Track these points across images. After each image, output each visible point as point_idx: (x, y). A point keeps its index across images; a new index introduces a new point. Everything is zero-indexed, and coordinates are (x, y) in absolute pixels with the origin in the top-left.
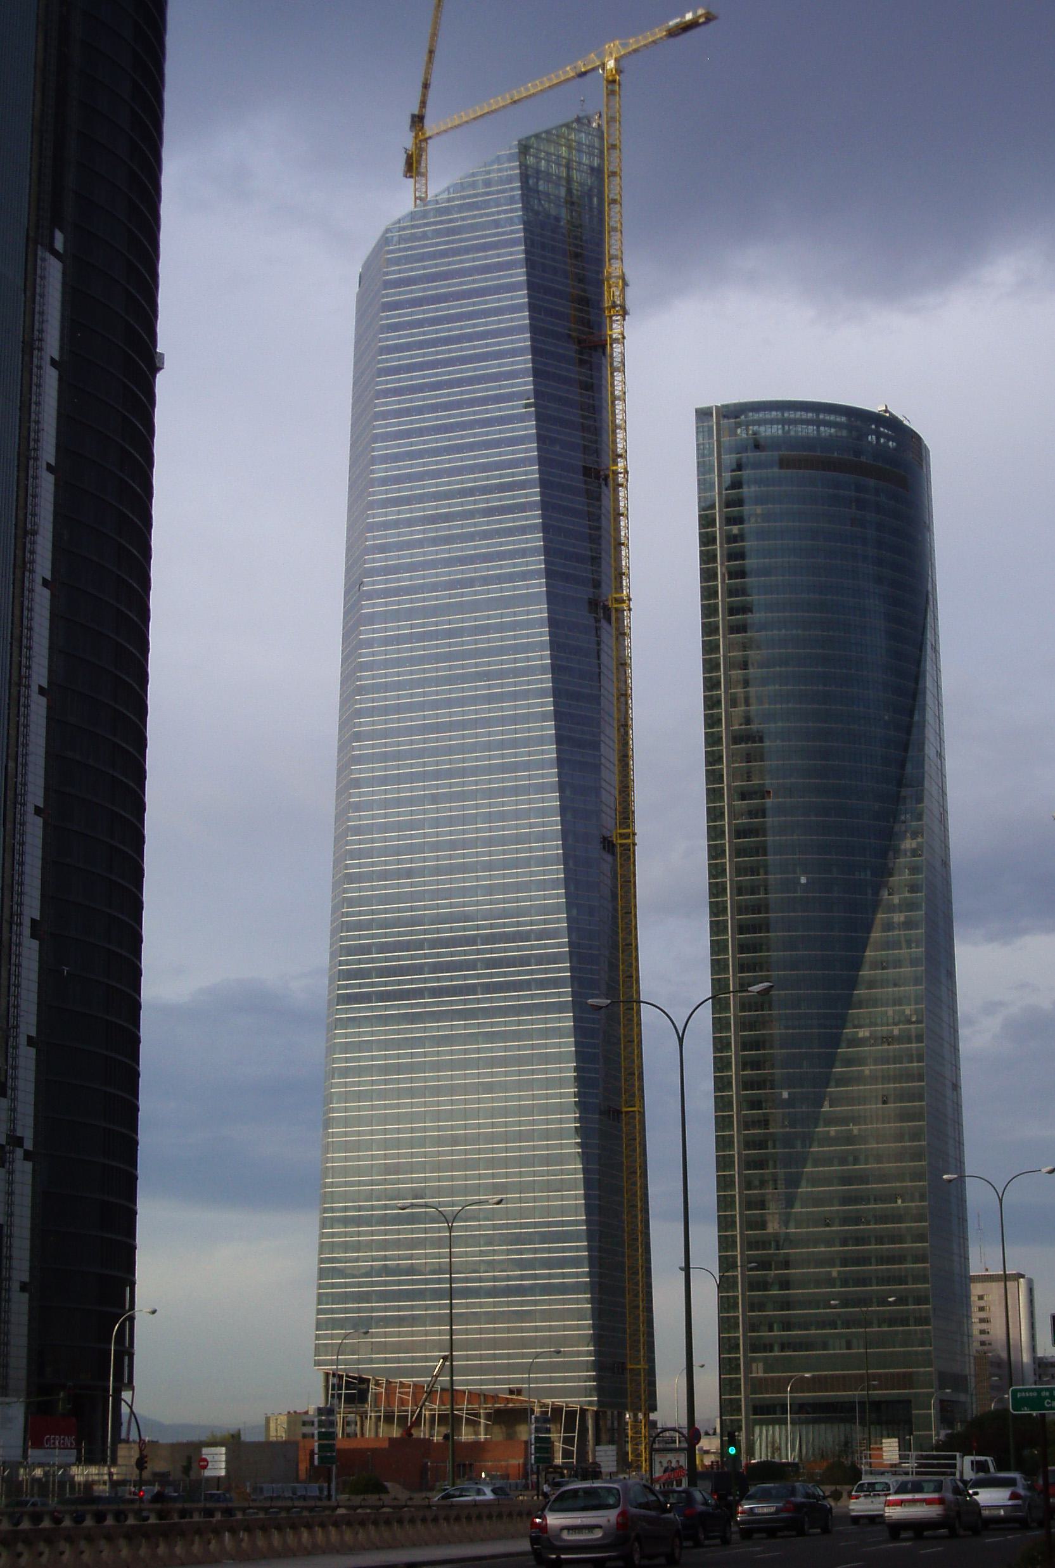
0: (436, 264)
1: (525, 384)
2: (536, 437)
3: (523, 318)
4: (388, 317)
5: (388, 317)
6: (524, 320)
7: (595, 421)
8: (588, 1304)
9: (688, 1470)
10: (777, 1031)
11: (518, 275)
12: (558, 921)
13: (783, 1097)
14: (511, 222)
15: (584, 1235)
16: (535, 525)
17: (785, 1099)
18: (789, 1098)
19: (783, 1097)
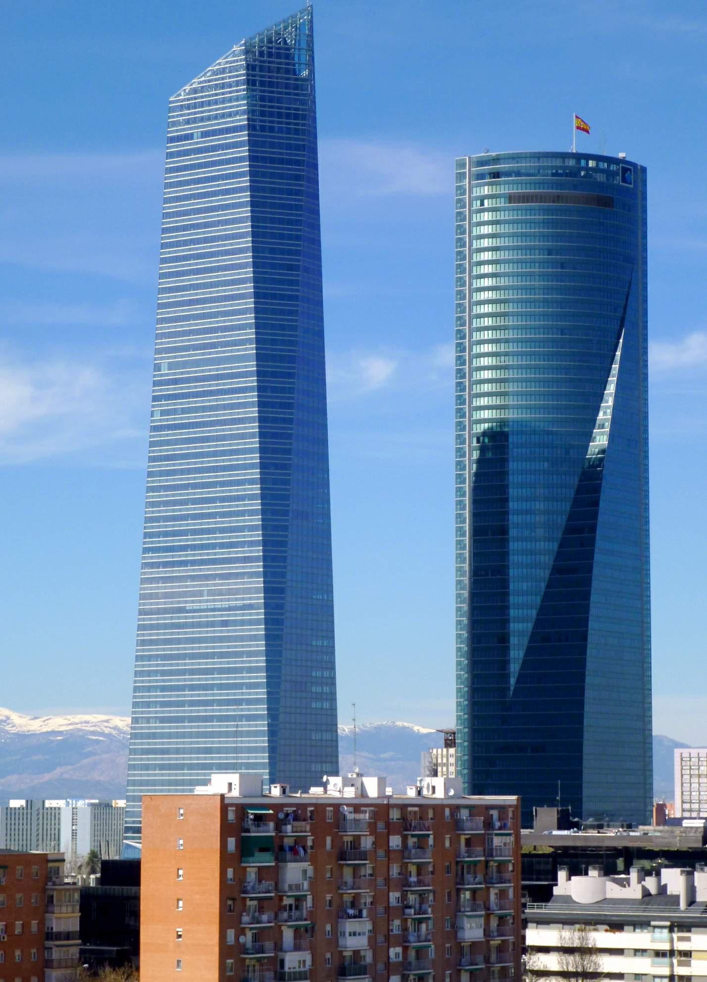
0: (249, 741)
1: (247, 242)
2: (256, 373)
3: (250, 318)
4: (162, 313)
5: (162, 313)
6: (264, 743)
7: (314, 160)
8: (243, 85)
9: (573, 828)
10: (525, 570)
11: (252, 412)
12: (258, 598)
13: (233, 930)
14: (237, 83)
15: (263, 621)
16: (244, 126)
17: (329, 836)
18: (325, 836)
19: (233, 930)
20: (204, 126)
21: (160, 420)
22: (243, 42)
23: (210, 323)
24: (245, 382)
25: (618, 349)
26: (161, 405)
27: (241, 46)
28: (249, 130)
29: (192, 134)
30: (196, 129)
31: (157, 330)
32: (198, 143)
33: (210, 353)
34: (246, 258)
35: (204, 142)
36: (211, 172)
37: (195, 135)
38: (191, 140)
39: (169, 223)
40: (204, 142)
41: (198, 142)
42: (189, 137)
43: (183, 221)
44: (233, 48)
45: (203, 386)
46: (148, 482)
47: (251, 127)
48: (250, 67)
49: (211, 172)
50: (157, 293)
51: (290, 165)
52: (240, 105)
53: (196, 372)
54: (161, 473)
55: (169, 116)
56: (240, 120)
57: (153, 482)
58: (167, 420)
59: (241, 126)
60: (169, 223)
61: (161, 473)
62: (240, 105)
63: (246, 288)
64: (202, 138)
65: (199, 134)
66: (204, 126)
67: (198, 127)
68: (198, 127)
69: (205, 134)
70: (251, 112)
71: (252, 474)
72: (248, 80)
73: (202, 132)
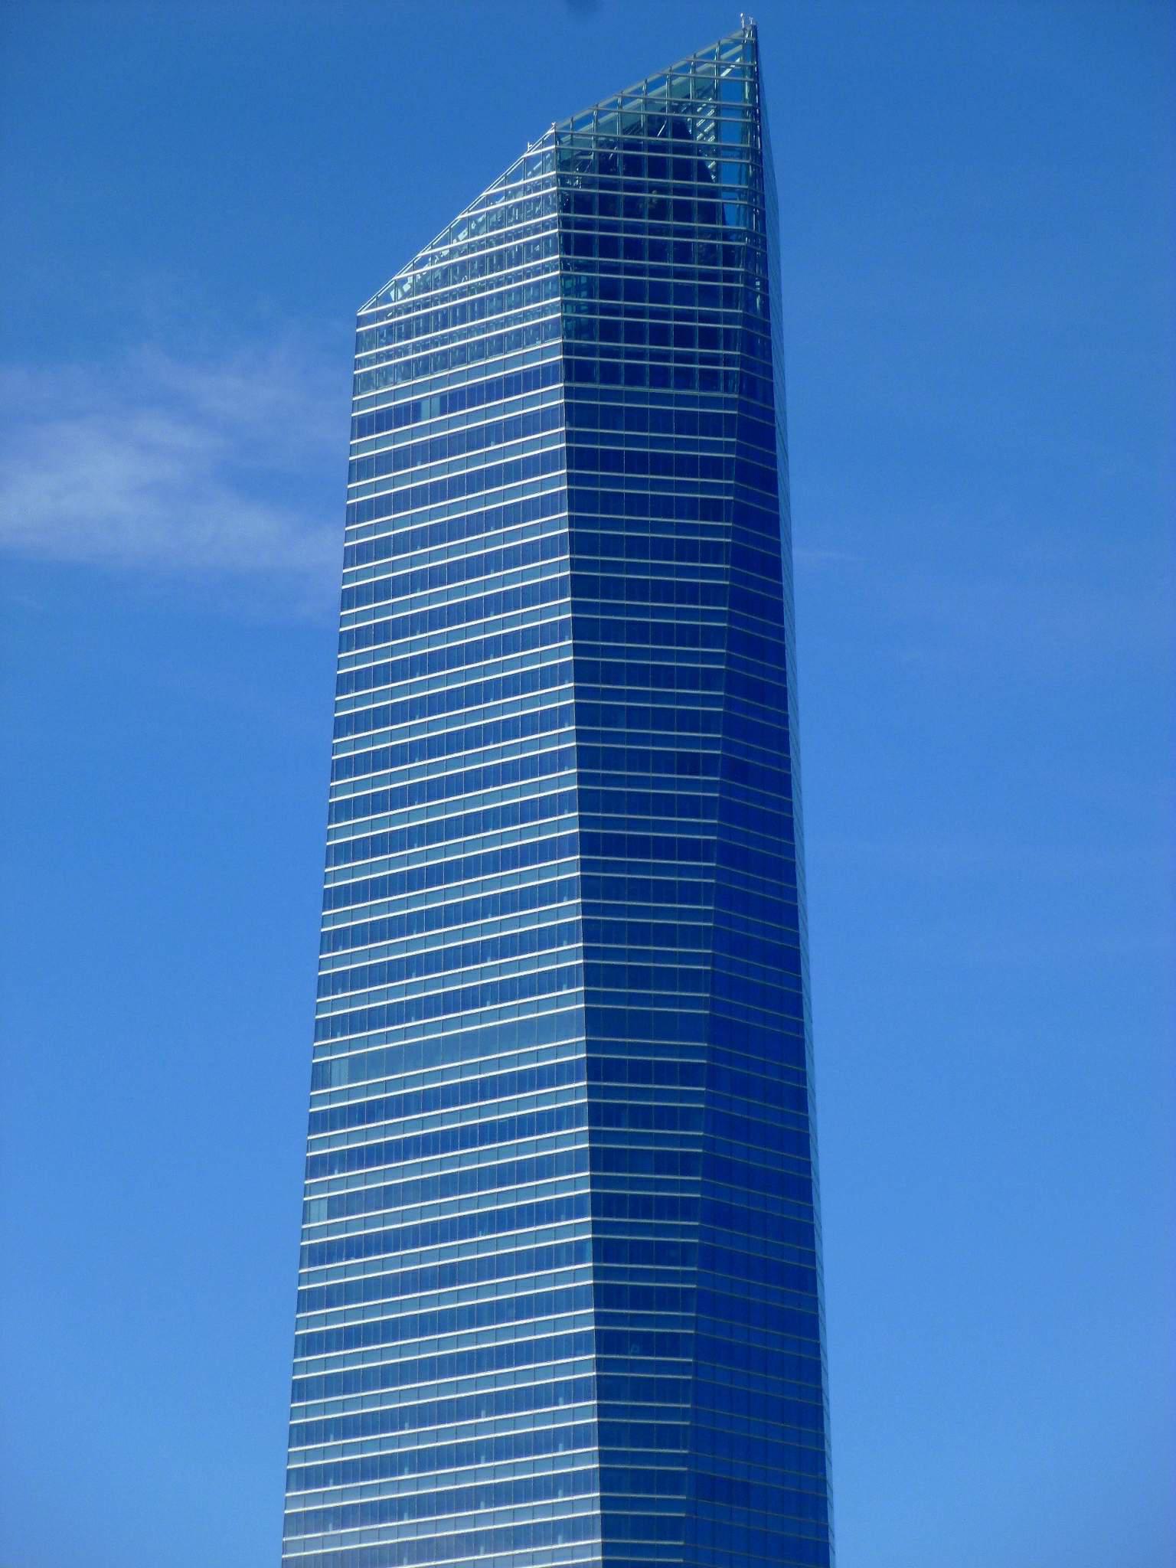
5: (335, 919)
20: (450, 380)
21: (329, 1230)
22: (551, 131)
23: (497, 1289)
24: (557, 1097)
25: (697, 168)
26: (329, 1186)
27: (546, 143)
28: (568, 378)
29: (417, 405)
30: (427, 389)
31: (284, 1552)
32: (431, 428)
33: (462, 1022)
34: (561, 738)
35: (449, 424)
36: (467, 548)
37: (425, 406)
38: (415, 421)
39: (356, 659)
40: (449, 424)
41: (433, 427)
42: (413, 412)
43: (394, 608)
44: (525, 150)
45: (457, 1432)
46: (293, 1413)
47: (575, 370)
48: (571, 203)
49: (467, 548)
50: (293, 1356)
51: (736, 571)
52: (544, 311)
53: (423, 1079)
54: (329, 1385)
55: (359, 360)
56: (543, 353)
57: (306, 1411)
58: (346, 1227)
59: (545, 368)
60: (356, 659)
61: (329, 1385)
62: (544, 311)
63: (559, 826)
64: (443, 413)
65: (437, 402)
66: (450, 380)
67: (431, 385)
68: (431, 385)
69: (451, 402)
70: (574, 329)
71: (574, 1368)
72: (566, 237)
73: (443, 397)
